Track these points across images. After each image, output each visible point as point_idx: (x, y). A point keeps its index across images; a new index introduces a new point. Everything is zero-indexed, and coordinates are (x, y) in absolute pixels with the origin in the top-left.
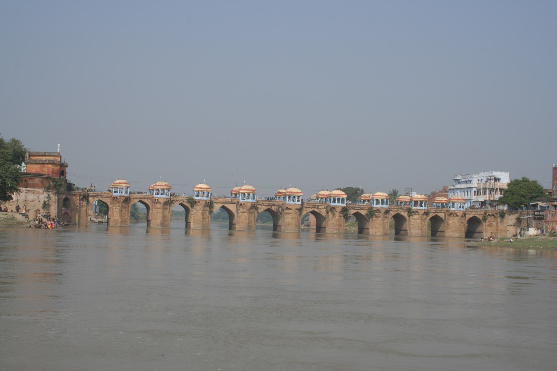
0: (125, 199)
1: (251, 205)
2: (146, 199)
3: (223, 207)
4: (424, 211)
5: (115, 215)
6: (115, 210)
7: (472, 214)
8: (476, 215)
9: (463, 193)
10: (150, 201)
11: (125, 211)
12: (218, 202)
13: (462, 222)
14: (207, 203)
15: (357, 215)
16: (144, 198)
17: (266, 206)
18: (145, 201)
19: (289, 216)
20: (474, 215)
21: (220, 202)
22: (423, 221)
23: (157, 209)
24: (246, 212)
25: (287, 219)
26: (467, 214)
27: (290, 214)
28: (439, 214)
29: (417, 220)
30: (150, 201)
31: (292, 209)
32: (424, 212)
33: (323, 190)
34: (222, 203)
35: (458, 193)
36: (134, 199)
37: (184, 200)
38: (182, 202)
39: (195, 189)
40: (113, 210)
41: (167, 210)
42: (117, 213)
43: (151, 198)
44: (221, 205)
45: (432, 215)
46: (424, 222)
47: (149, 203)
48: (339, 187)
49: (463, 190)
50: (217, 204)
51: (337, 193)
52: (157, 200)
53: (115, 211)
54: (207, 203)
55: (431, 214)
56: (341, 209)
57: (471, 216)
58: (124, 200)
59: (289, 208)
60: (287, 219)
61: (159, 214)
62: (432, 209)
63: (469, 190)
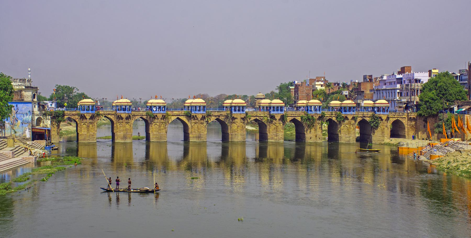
0: (91, 116)
1: (202, 117)
2: (110, 115)
3: (178, 118)
4: (352, 116)
5: (84, 130)
6: (83, 126)
7: (395, 117)
8: (398, 118)
9: (388, 94)
10: (113, 116)
11: (92, 126)
12: (174, 114)
13: (386, 126)
14: (164, 116)
15: (294, 121)
16: (109, 114)
17: (214, 117)
18: (109, 116)
19: (235, 125)
20: (396, 119)
21: (175, 114)
22: (351, 125)
23: (120, 123)
24: (198, 123)
25: (233, 127)
26: (391, 117)
27: (236, 123)
28: (297, 118)
29: (347, 125)
30: (114, 116)
31: (237, 119)
32: (353, 117)
33: (121, 98)
34: (177, 115)
35: (384, 94)
36: (136, 116)
37: (143, 114)
38: (142, 116)
39: (186, 104)
40: (81, 126)
41: (129, 124)
42: (85, 128)
43: (114, 114)
44: (177, 117)
45: (360, 119)
46: (352, 126)
47: (113, 118)
48: (223, 93)
49: (387, 91)
50: (112, 115)
51: (90, 102)
52: (120, 115)
53: (83, 127)
54: (164, 116)
55: (359, 118)
56: (280, 117)
57: (395, 119)
58: (90, 117)
59: (235, 117)
60: (233, 127)
61: (122, 127)
62: (359, 114)
63: (393, 91)
